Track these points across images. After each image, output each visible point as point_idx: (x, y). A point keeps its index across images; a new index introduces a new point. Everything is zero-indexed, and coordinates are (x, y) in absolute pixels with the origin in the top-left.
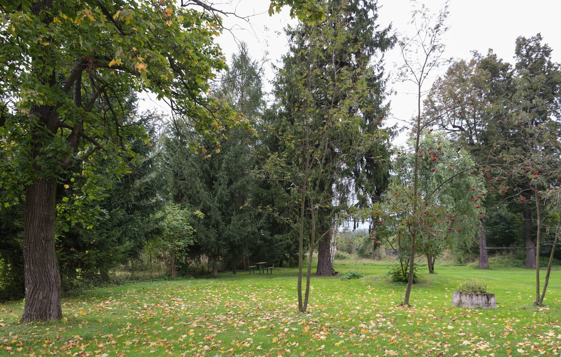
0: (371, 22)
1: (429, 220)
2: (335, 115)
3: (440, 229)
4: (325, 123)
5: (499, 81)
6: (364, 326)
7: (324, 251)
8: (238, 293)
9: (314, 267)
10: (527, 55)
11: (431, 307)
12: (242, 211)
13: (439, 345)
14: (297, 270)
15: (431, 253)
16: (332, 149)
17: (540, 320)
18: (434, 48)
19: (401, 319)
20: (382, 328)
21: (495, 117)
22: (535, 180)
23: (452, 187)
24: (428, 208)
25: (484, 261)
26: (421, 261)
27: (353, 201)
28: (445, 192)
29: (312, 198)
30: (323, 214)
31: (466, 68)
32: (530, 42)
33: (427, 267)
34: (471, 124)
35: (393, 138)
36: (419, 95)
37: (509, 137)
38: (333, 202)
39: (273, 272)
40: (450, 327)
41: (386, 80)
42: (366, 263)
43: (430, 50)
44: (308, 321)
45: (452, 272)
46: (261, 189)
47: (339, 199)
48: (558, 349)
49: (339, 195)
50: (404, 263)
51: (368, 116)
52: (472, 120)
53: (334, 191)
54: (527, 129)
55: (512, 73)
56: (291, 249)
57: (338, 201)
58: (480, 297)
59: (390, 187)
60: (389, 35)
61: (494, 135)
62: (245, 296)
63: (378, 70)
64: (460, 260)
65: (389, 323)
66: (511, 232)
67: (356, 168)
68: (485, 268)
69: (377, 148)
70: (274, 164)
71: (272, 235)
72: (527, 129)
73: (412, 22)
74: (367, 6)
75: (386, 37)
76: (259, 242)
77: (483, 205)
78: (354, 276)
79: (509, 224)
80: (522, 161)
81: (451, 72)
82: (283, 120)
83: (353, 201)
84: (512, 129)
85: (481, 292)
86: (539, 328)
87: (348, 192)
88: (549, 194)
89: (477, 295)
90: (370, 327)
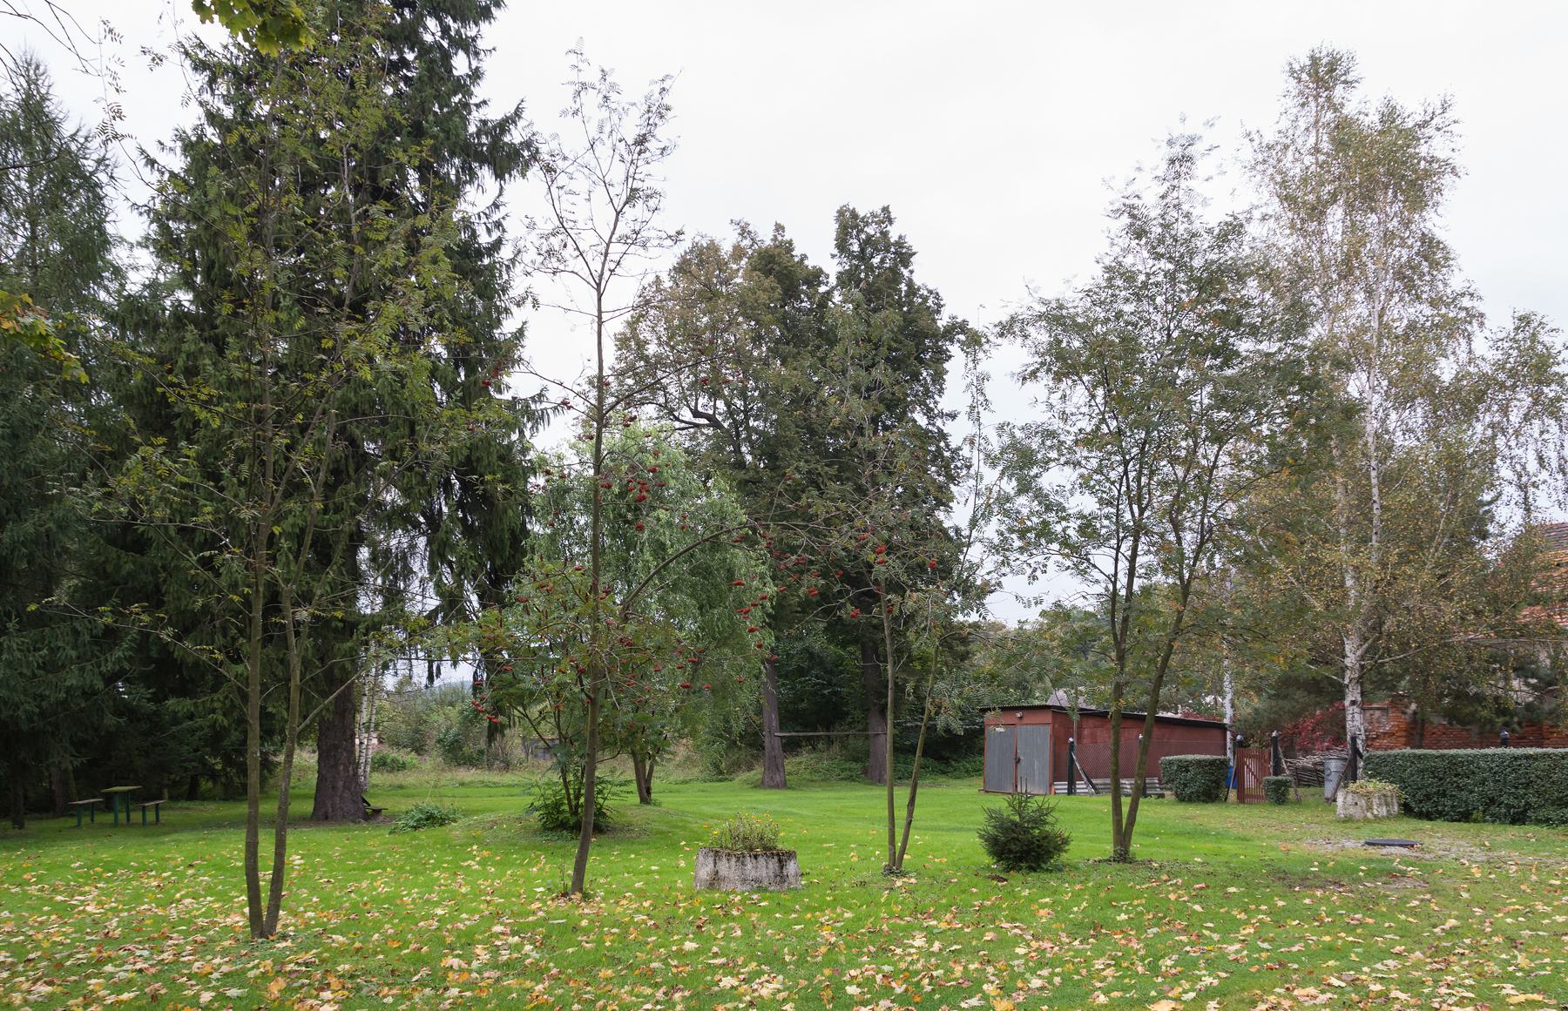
0: (461, 86)
1: (634, 662)
2: (354, 344)
3: (664, 685)
4: (322, 363)
5: (799, 310)
6: (455, 962)
7: (336, 747)
8: (33, 890)
9: (305, 797)
10: (862, 257)
11: (641, 895)
12: (40, 620)
13: (660, 995)
14: (243, 809)
15: (644, 749)
16: (354, 443)
17: (897, 909)
18: (632, 196)
19: (562, 934)
20: (508, 965)
21: (792, 402)
22: (886, 568)
23: (693, 573)
24: (631, 628)
25: (775, 767)
26: (616, 771)
27: (423, 600)
28: (675, 587)
29: (288, 590)
30: (331, 635)
31: (721, 265)
32: (867, 224)
33: (634, 787)
34: (738, 411)
35: (534, 428)
36: (600, 317)
37: (827, 455)
38: (363, 601)
39: (165, 816)
40: (689, 946)
41: (513, 261)
42: (467, 780)
43: (624, 198)
44: (280, 962)
45: (699, 799)
46: (113, 552)
47: (381, 592)
48: (932, 977)
49: (379, 581)
50: (570, 777)
51: (460, 356)
52: (739, 403)
53: (364, 567)
54: (860, 440)
55: (829, 294)
56: (226, 742)
57: (379, 600)
58: (762, 860)
59: (528, 566)
60: (515, 136)
61: (790, 447)
62: (59, 898)
63: (489, 231)
64: (716, 766)
65: (528, 948)
66: (835, 693)
67: (432, 504)
68: (777, 786)
69: (489, 453)
70: (151, 475)
71: (158, 699)
72: (860, 440)
73: (575, 113)
74: (450, 38)
75: (507, 139)
76: (110, 720)
77: (769, 625)
78: (432, 820)
79: (831, 672)
80: (851, 520)
81: (682, 268)
82: (188, 336)
83: (423, 600)
84: (831, 436)
85: (765, 848)
86: (894, 929)
87: (408, 573)
88: (910, 604)
89: (756, 857)
90: (475, 964)
